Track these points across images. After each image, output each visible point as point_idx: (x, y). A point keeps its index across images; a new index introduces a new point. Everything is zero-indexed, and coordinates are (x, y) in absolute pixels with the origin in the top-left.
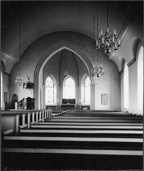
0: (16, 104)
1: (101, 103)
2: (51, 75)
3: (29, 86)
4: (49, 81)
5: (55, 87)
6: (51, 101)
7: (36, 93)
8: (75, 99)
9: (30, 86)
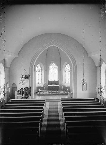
0: (16, 92)
1: (82, 90)
2: (40, 63)
3: (27, 78)
4: (39, 67)
5: (42, 71)
6: (40, 82)
7: (31, 83)
8: (58, 81)
9: (27, 77)
